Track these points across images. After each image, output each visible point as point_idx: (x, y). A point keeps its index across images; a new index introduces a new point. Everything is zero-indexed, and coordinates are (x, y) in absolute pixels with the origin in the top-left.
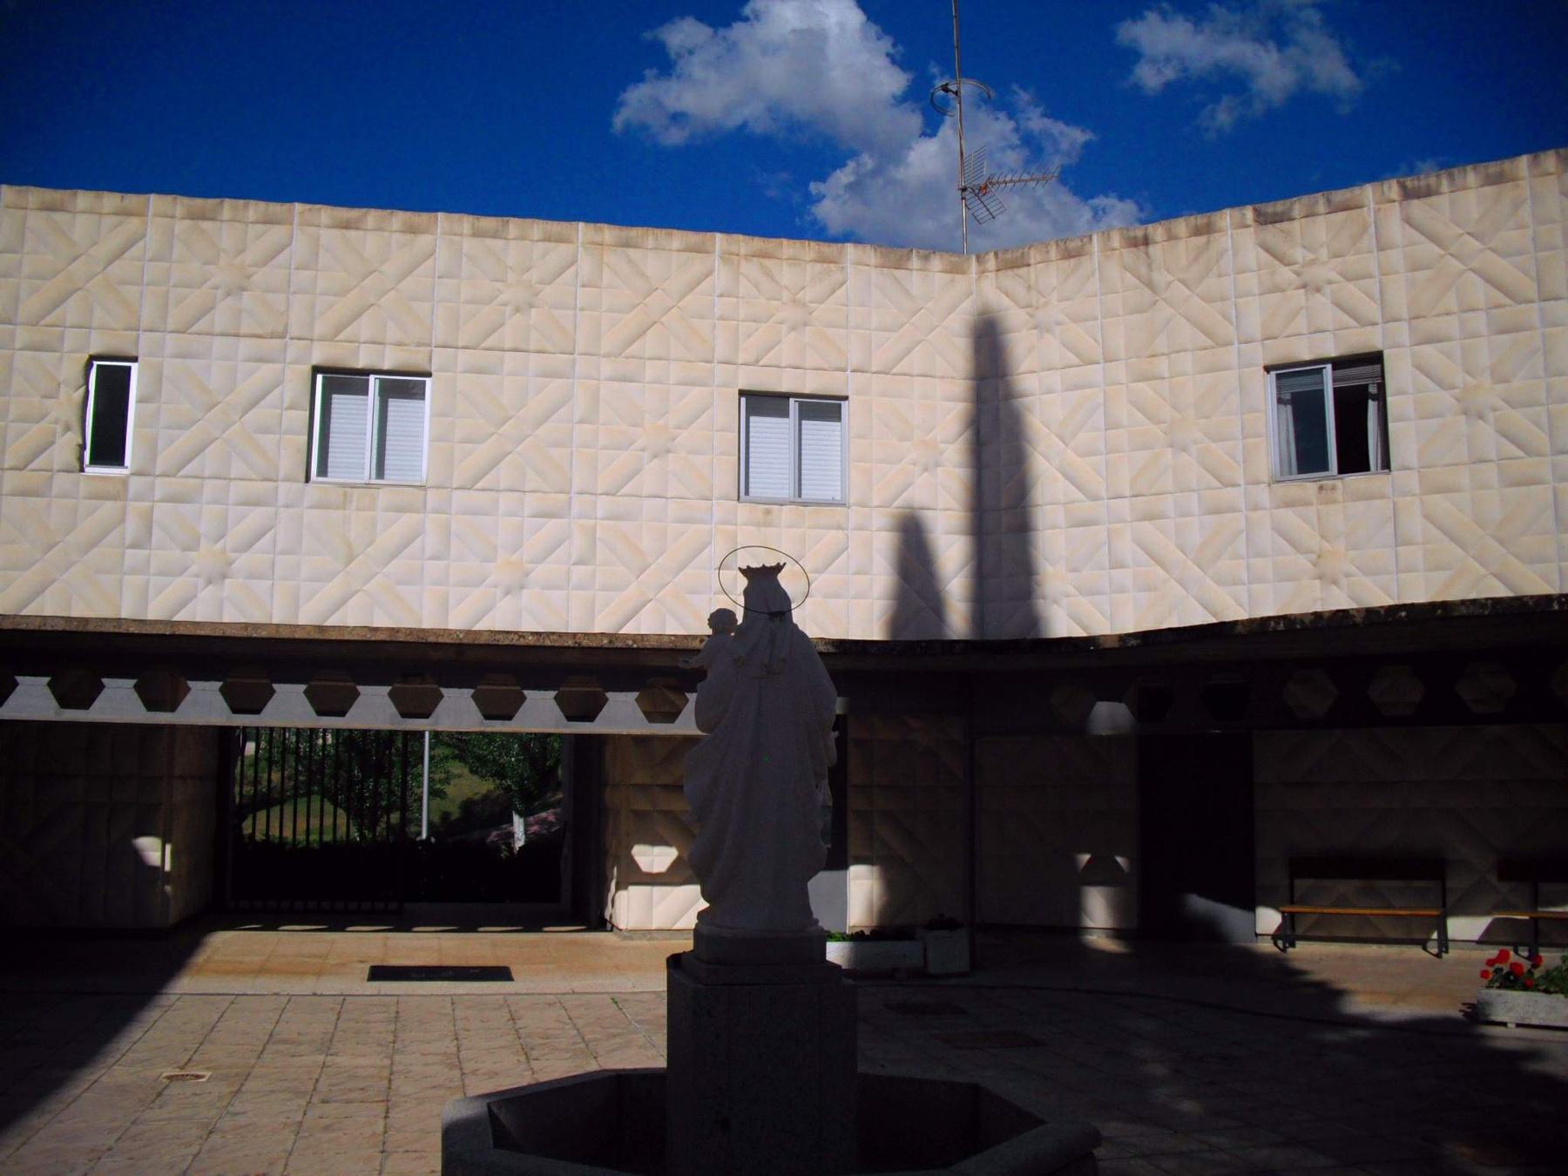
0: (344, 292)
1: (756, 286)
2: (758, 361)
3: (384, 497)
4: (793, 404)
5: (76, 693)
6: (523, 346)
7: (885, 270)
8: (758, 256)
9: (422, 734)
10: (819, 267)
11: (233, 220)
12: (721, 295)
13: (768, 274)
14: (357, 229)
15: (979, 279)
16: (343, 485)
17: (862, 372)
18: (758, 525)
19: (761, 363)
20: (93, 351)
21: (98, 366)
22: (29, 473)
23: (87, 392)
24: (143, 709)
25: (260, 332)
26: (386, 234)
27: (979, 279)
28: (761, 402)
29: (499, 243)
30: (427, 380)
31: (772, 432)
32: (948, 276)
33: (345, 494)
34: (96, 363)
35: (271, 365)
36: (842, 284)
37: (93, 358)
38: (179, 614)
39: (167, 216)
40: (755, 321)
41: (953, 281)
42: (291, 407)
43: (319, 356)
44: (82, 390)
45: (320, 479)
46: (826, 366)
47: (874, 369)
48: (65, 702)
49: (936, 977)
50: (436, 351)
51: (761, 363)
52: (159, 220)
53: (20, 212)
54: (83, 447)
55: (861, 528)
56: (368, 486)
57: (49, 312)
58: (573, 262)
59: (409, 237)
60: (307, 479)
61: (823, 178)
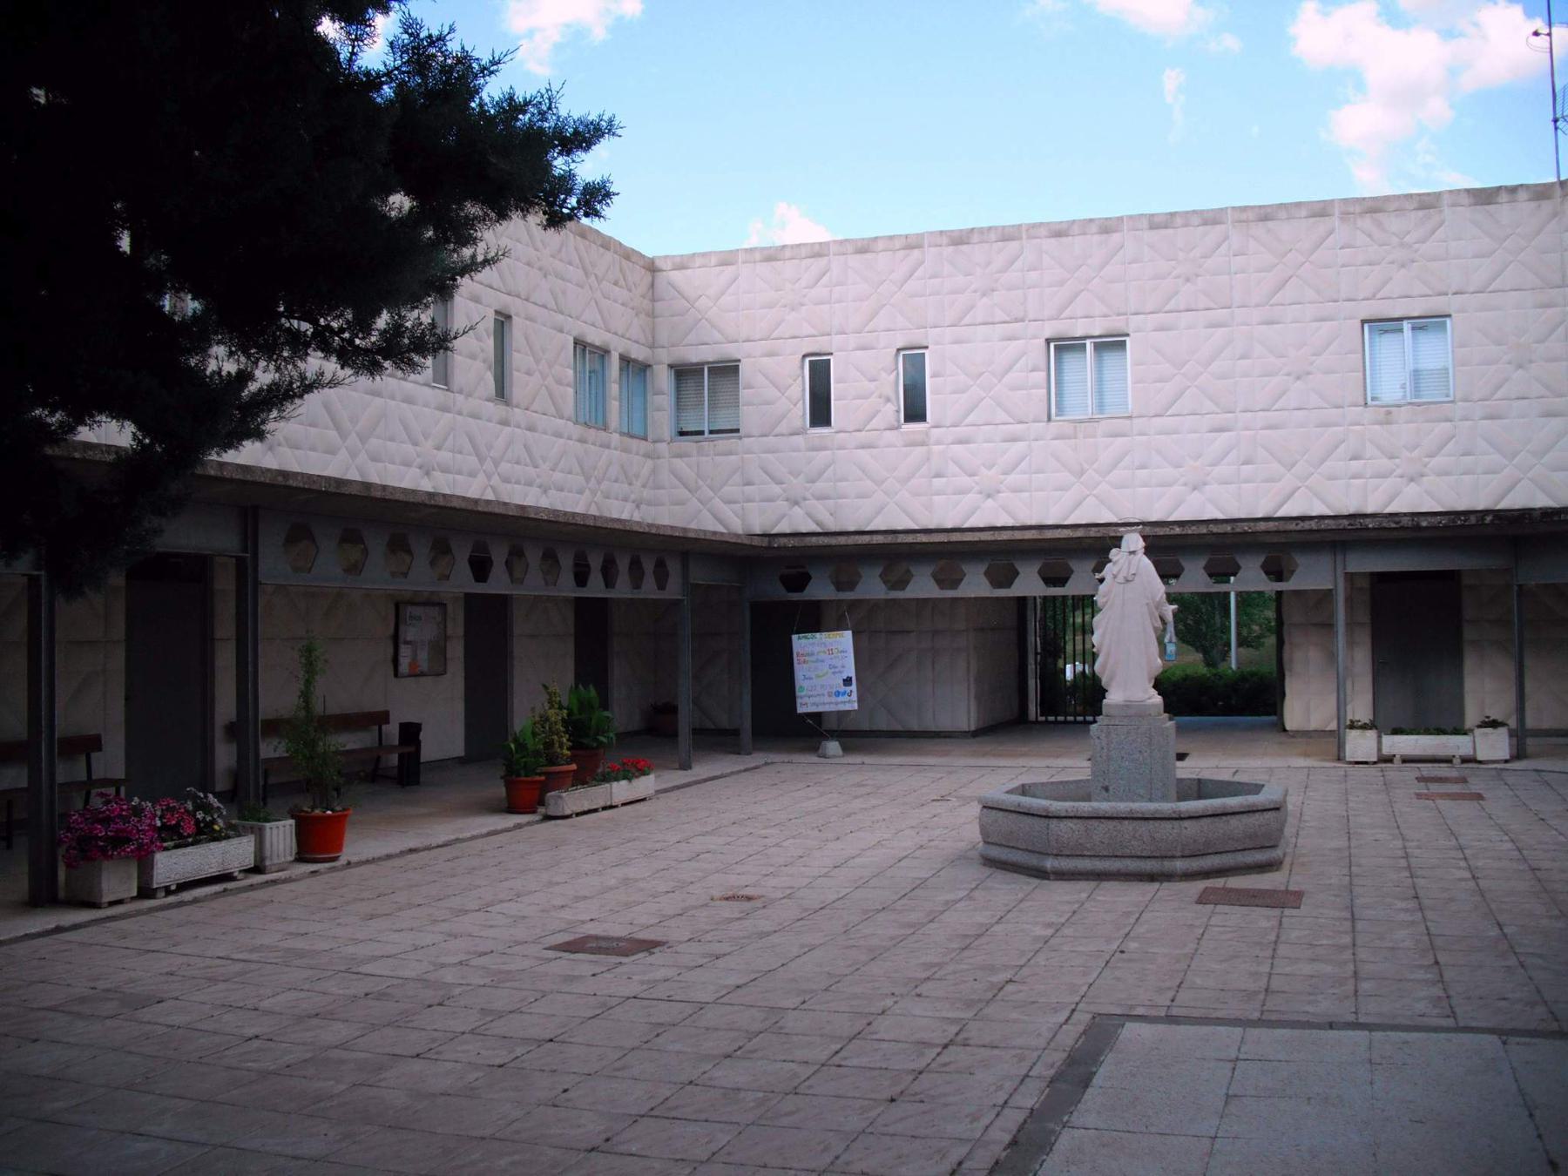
0: (1062, 283)
1: (1370, 236)
2: (1374, 296)
3: (1103, 426)
4: (1089, 344)
5: (949, 579)
6: (1193, 307)
7: (1478, 207)
8: (1370, 212)
9: (1227, 595)
10: (1421, 213)
11: (981, 242)
12: (1342, 248)
13: (1379, 225)
14: (1067, 236)
15: (1562, 203)
16: (1074, 421)
17: (1462, 293)
18: (1380, 423)
19: (1378, 296)
20: (900, 345)
21: (810, 361)
22: (965, 428)
23: (898, 374)
24: (936, 587)
25: (1008, 319)
26: (1089, 236)
27: (1562, 203)
28: (1065, 346)
29: (1170, 231)
30: (1127, 339)
31: (1082, 367)
32: (1533, 204)
33: (1075, 427)
34: (807, 360)
35: (1223, 329)
36: (1441, 225)
37: (805, 356)
38: (1392, 505)
39: (937, 246)
40: (1370, 264)
41: (1539, 206)
42: (1351, 352)
43: (1050, 330)
44: (895, 373)
45: (1058, 418)
46: (1430, 293)
47: (1472, 290)
48: (996, 584)
49: (1480, 762)
50: (1237, 311)
51: (1378, 296)
52: (932, 249)
53: (842, 258)
54: (898, 411)
55: (1466, 419)
56: (1090, 420)
57: (867, 325)
58: (1226, 238)
59: (1104, 237)
60: (1049, 419)
61: (547, 220)
